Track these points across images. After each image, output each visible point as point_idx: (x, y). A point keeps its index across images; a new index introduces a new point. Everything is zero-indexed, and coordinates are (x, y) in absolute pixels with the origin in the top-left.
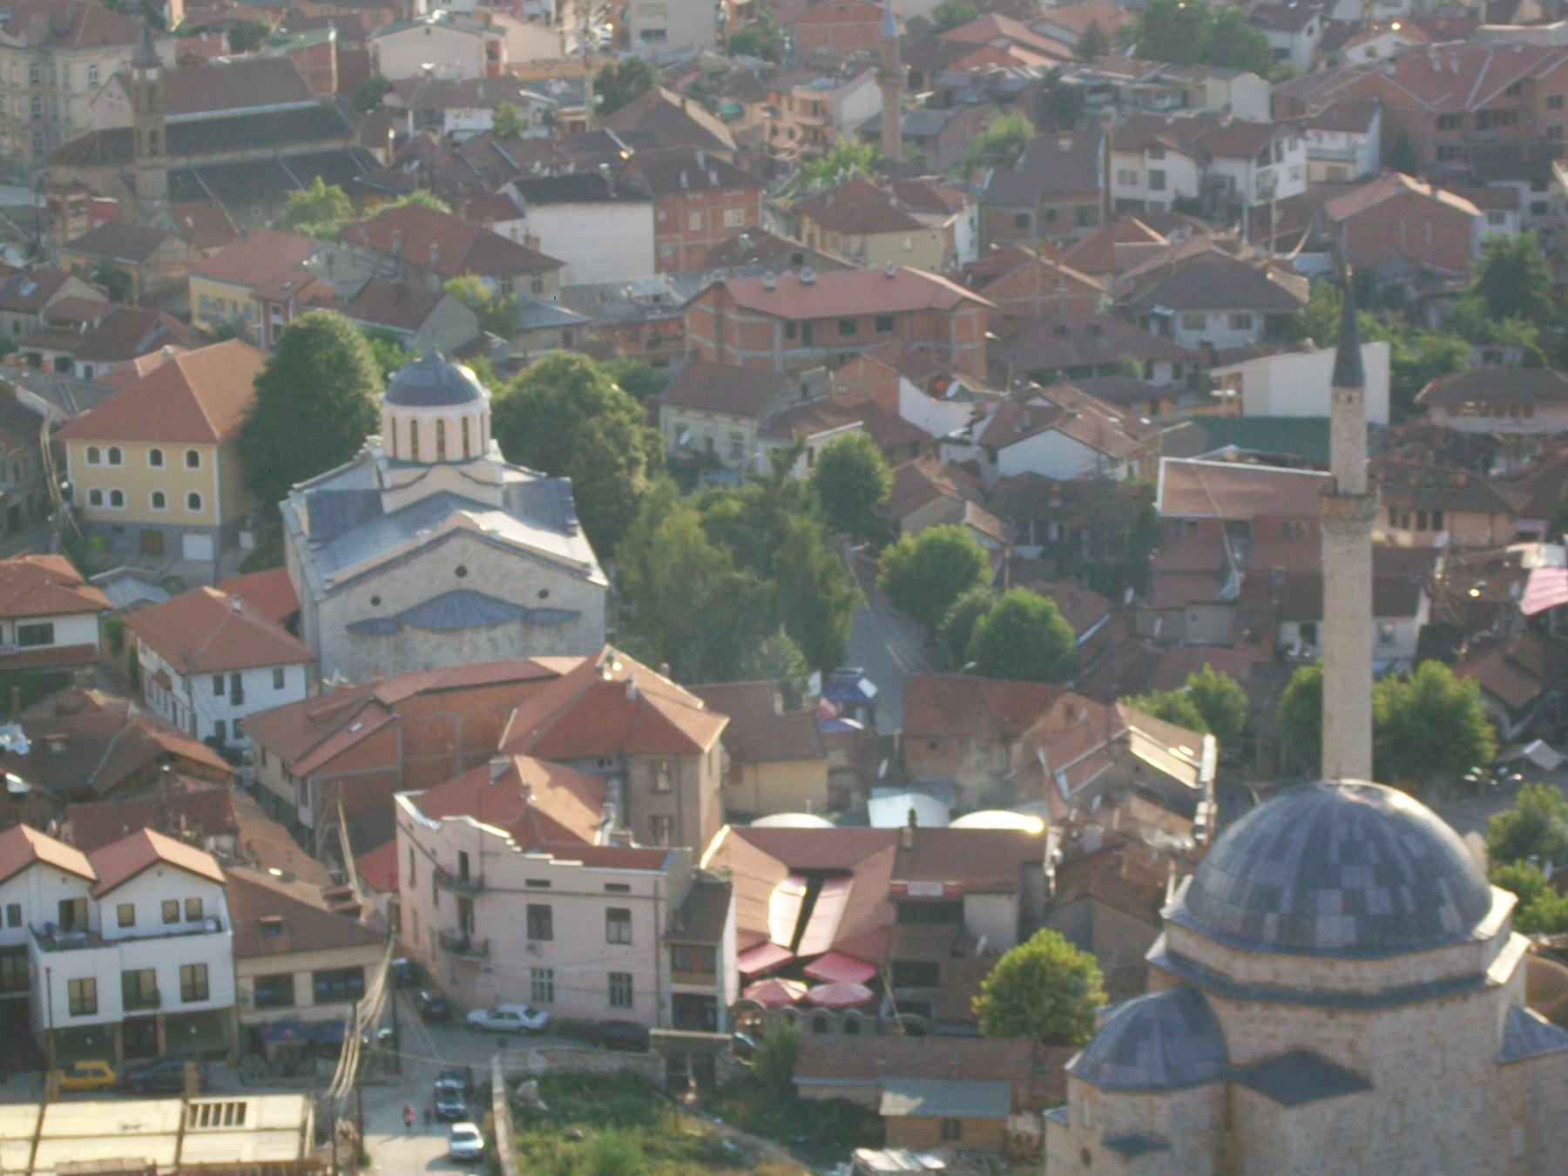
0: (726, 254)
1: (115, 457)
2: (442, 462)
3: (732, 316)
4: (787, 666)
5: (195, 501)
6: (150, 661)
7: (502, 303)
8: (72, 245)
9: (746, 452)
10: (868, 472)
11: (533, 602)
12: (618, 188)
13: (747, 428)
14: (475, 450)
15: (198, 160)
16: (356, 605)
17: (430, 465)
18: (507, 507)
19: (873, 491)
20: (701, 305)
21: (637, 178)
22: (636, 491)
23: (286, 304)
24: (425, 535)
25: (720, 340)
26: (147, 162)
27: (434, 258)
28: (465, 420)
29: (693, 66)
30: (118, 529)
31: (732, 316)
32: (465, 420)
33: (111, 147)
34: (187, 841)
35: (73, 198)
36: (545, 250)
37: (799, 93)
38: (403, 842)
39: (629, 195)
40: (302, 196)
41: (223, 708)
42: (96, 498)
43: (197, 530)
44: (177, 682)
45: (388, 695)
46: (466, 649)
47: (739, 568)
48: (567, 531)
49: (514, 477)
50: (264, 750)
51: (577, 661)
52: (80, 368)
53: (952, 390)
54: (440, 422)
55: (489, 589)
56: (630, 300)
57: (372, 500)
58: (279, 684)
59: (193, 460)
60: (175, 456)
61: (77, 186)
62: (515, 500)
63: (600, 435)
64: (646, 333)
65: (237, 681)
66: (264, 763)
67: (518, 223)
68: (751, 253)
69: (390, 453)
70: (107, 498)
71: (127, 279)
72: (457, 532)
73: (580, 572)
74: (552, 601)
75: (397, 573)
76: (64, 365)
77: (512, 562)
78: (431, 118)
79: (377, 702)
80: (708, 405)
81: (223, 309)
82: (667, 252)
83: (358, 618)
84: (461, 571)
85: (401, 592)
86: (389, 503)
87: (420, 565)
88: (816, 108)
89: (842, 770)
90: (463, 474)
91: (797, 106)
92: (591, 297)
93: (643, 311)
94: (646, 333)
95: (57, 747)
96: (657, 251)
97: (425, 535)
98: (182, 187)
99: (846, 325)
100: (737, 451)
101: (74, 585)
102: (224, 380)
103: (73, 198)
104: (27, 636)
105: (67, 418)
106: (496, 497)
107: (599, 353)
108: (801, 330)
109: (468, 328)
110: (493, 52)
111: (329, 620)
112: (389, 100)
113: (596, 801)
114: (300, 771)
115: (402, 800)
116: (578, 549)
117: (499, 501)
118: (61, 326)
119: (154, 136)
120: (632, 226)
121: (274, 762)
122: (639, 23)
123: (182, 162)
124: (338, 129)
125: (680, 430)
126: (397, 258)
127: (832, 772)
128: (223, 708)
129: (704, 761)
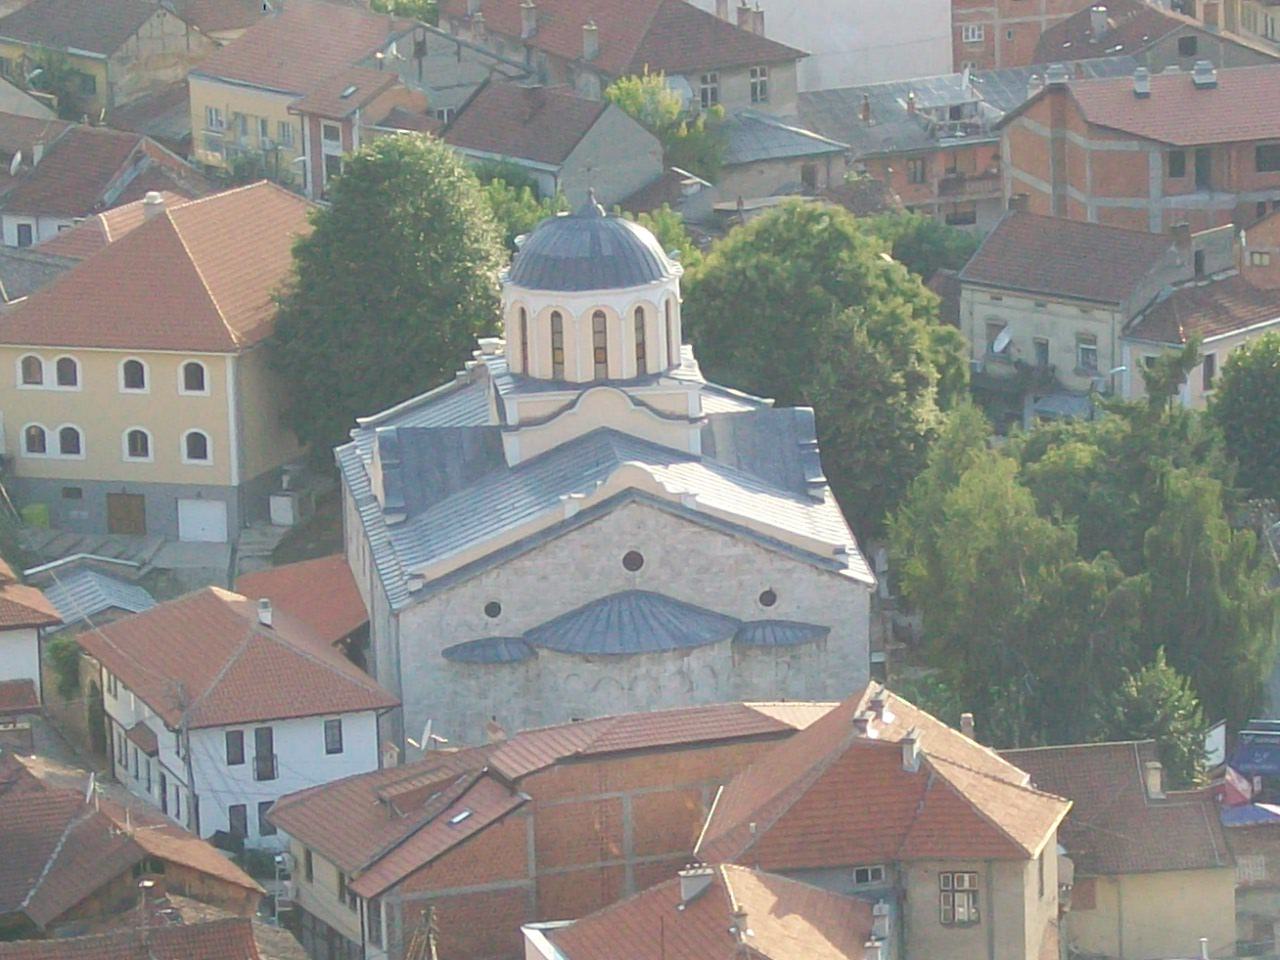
1: (67, 373)
2: (602, 381)
3: (1078, 139)
4: (1167, 718)
5: (197, 446)
6: (122, 707)
9: (1103, 365)
13: (1104, 324)
14: (656, 362)
16: (462, 615)
18: (707, 455)
20: (1027, 122)
23: (348, 121)
24: (573, 502)
25: (1059, 182)
27: (589, 47)
28: (639, 311)
30: (73, 492)
31: (1078, 139)
32: (639, 311)
36: (773, 32)
41: (243, 785)
43: (200, 493)
44: (166, 740)
45: (511, 764)
46: (641, 689)
48: (805, 494)
49: (718, 405)
51: (823, 709)
54: (599, 315)
55: (680, 591)
57: (489, 443)
58: (335, 747)
63: (861, 337)
65: (265, 739)
68: (1111, 37)
69: (518, 369)
70: (53, 440)
71: (88, 82)
72: (628, 495)
73: (828, 562)
75: (527, 563)
77: (718, 546)
79: (493, 774)
80: (1042, 288)
82: (973, 35)
84: (633, 561)
86: (515, 449)
89: (1260, 887)
90: (638, 403)
93: (932, 132)
94: (938, 169)
96: (956, 34)
97: (573, 502)
100: (1087, 363)
102: (246, 248)
107: (860, 201)
108: (1193, 164)
109: (648, 163)
111: (415, 640)
114: (367, 888)
115: (533, 935)
116: (823, 523)
117: (696, 450)
121: (326, 874)
125: (995, 327)
127: (1243, 891)
128: (243, 785)
129: (1032, 868)
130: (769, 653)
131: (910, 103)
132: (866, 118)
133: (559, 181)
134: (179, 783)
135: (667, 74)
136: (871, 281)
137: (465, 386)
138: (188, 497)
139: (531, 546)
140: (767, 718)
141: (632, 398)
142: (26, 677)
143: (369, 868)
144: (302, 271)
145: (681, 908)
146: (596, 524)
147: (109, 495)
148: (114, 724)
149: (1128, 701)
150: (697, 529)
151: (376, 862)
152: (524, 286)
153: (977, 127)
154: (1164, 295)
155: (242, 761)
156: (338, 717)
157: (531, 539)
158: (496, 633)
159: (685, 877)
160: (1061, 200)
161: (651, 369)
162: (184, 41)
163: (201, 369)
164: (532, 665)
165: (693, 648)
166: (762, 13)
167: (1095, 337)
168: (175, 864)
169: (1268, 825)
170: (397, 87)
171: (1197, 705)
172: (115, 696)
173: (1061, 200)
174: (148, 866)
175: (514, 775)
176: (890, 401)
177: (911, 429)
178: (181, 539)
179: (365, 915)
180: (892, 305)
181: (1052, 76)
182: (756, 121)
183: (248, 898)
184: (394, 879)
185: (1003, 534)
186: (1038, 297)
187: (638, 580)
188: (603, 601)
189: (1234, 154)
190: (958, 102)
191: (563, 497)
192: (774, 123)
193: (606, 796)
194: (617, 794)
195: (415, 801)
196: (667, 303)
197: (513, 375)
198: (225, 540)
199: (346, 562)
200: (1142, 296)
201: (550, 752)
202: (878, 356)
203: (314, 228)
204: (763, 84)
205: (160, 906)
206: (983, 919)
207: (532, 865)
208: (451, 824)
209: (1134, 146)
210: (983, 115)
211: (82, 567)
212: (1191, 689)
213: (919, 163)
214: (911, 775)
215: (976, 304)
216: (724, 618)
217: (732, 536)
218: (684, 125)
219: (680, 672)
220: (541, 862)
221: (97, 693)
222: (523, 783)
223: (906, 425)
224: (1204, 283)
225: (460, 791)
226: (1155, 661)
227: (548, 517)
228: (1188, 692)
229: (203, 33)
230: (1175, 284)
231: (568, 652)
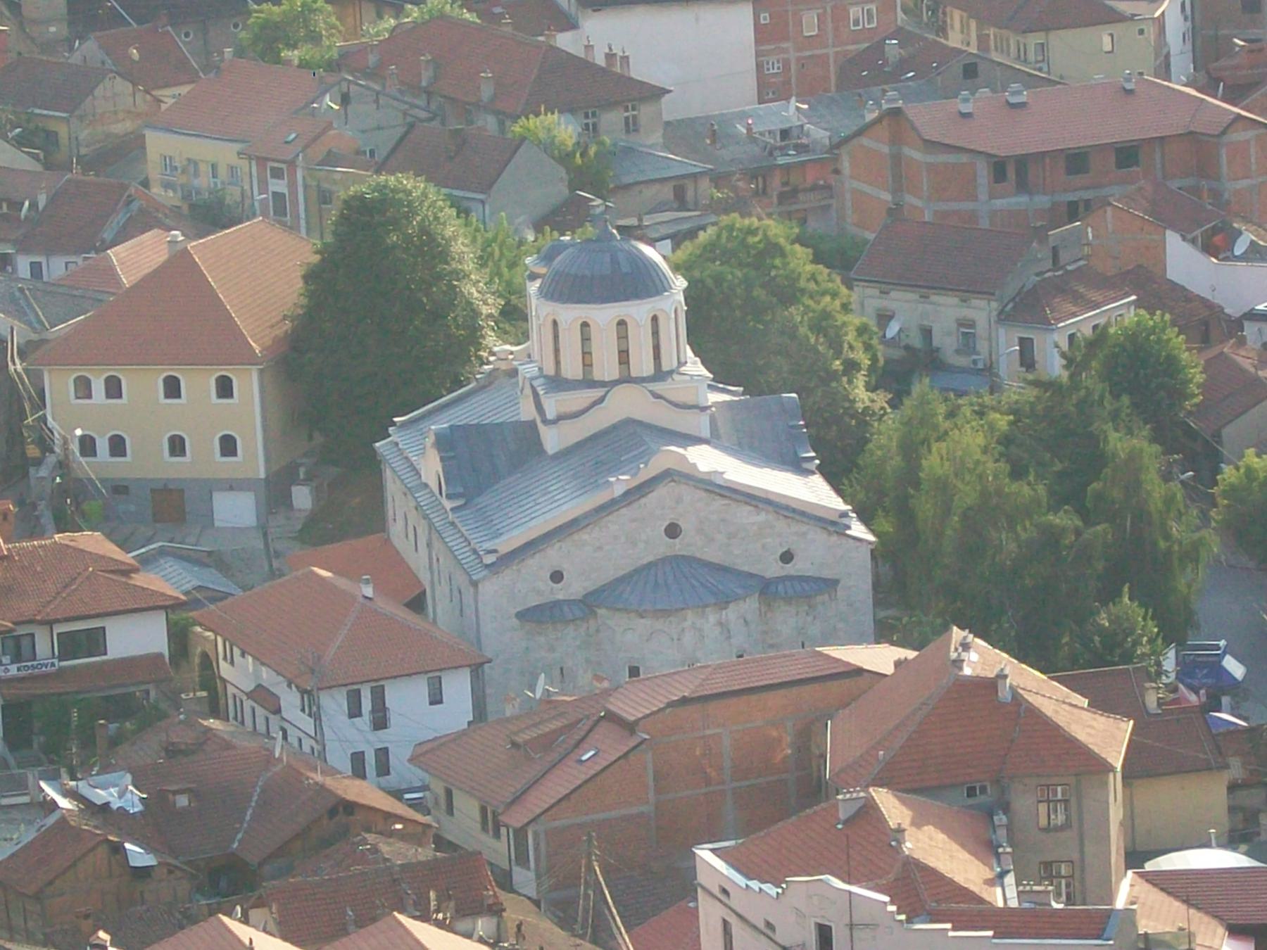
1: (114, 388)
2: (626, 379)
3: (914, 154)
4: (1136, 643)
5: (228, 446)
6: (239, 673)
7: (593, 150)
9: (982, 346)
10: (1171, 366)
11: (774, 569)
13: (982, 311)
16: (529, 585)
17: (615, 383)
18: (713, 439)
19: (1179, 394)
20: (865, 141)
22: (860, 406)
23: (292, 164)
24: (621, 482)
25: (897, 190)
27: (486, 92)
28: (655, 319)
30: (120, 489)
31: (914, 154)
32: (655, 319)
34: (440, 925)
36: (640, 71)
38: (709, 915)
42: (88, 446)
43: (232, 486)
46: (689, 639)
47: (1054, 508)
48: (798, 466)
49: (714, 398)
50: (449, 793)
52: (23, 265)
53: (1240, 248)
54: (622, 323)
55: (712, 554)
57: (527, 436)
58: (436, 699)
59: (225, 388)
60: (199, 384)
63: (803, 330)
64: (776, 182)
65: (379, 697)
66: (450, 810)
68: (903, 65)
69: (550, 370)
70: (103, 446)
72: (666, 475)
74: (799, 567)
75: (584, 536)
77: (745, 516)
79: (612, 717)
80: (925, 283)
81: (196, 174)
83: (533, 601)
84: (673, 531)
85: (590, 562)
86: (552, 440)
90: (657, 396)
92: (698, 134)
94: (776, 182)
95: (183, 801)
96: (759, 66)
97: (621, 482)
99: (1076, 161)
100: (968, 341)
101: (127, 572)
102: (262, 274)
104: (71, 645)
105: (34, 337)
106: (701, 424)
109: (555, 189)
113: (987, 849)
114: (516, 818)
115: (704, 854)
116: (815, 491)
117: (706, 433)
121: (467, 808)
125: (884, 318)
127: (1232, 788)
130: (790, 604)
131: (749, 129)
132: (713, 142)
133: (487, 207)
134: (302, 735)
135: (560, 112)
136: (802, 283)
137: (484, 387)
138: (221, 490)
139: (586, 522)
140: (838, 660)
141: (650, 391)
142: (156, 651)
143: (513, 802)
144: (311, 295)
145: (840, 826)
146: (643, 500)
147: (152, 490)
148: (230, 688)
149: (1101, 630)
150: (727, 502)
151: (518, 798)
152: (556, 301)
153: (807, 146)
154: (1029, 286)
155: (360, 714)
156: (437, 674)
157: (586, 515)
158: (560, 597)
159: (843, 800)
161: (665, 368)
162: (131, 99)
163: (119, 381)
164: (592, 622)
165: (728, 603)
166: (627, 57)
167: (974, 322)
168: (363, 806)
169: (1232, 732)
170: (332, 132)
171: (1158, 633)
172: (232, 663)
174: (341, 809)
175: (632, 718)
176: (834, 384)
177: (852, 407)
178: (217, 524)
179: (512, 843)
180: (822, 304)
181: (888, 101)
182: (631, 148)
183: (424, 833)
184: (538, 811)
185: (984, 495)
186: (883, 286)
187: (677, 547)
188: (650, 565)
189: (1047, 160)
190: (786, 126)
191: (612, 479)
192: (644, 150)
193: (708, 732)
194: (719, 730)
195: (547, 743)
196: (676, 311)
197: (546, 377)
198: (254, 524)
199: (388, 541)
200: (1011, 289)
201: (661, 698)
202: (820, 348)
203: (318, 257)
204: (634, 117)
205: (359, 844)
206: (1075, 824)
207: (651, 794)
208: (581, 762)
209: (964, 158)
210: (808, 135)
211: (162, 552)
212: (1152, 619)
213: (760, 179)
214: (1004, 705)
216: (752, 575)
217: (756, 507)
218: (578, 155)
219: (720, 624)
220: (658, 791)
221: (207, 663)
222: (641, 723)
223: (847, 405)
224: (1060, 273)
225: (583, 733)
226: (1120, 595)
227: (600, 497)
228: (1150, 623)
229: (147, 92)
230: (1037, 275)
231: (626, 610)
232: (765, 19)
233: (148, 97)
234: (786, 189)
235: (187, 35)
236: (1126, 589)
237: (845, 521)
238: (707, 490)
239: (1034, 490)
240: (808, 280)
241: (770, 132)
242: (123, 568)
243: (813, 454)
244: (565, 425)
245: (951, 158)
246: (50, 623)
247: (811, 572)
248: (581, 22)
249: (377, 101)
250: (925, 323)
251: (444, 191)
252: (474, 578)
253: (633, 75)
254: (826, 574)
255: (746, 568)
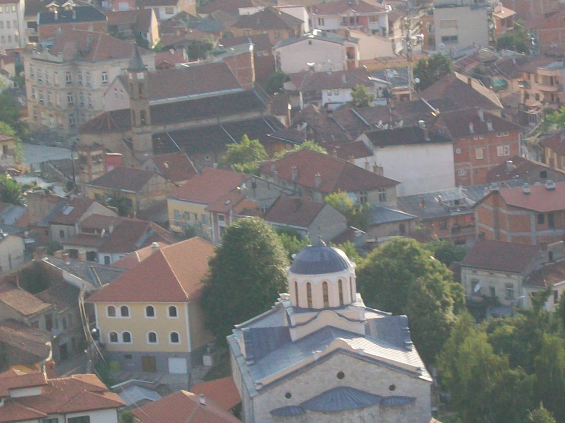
0: (500, 173)
1: (125, 312)
2: (327, 308)
3: (503, 211)
5: (175, 337)
8: (95, 183)
9: (516, 295)
11: (386, 393)
12: (430, 135)
13: (516, 280)
14: (347, 300)
15: (171, 127)
16: (276, 398)
18: (367, 335)
21: (442, 128)
22: (448, 322)
23: (228, 214)
24: (317, 354)
26: (139, 130)
27: (318, 182)
28: (340, 281)
29: (475, 57)
30: (128, 356)
31: (503, 211)
32: (340, 281)
33: (117, 121)
35: (94, 153)
36: (387, 174)
37: (542, 72)
39: (437, 139)
40: (236, 147)
42: (114, 338)
43: (177, 355)
49: (371, 316)
52: (101, 258)
54: (325, 283)
55: (358, 386)
56: (441, 204)
57: (285, 332)
59: (173, 312)
61: (96, 146)
62: (372, 330)
63: (424, 288)
67: (369, 159)
68: (514, 172)
69: (294, 304)
70: (120, 337)
71: (129, 202)
72: (338, 351)
73: (414, 373)
74: (398, 392)
75: (300, 377)
76: (91, 256)
77: (373, 369)
78: (314, 96)
81: (189, 219)
82: (463, 173)
83: (278, 406)
84: (341, 375)
85: (304, 389)
86: (295, 335)
87: (315, 372)
88: (552, 81)
90: (340, 315)
91: (540, 80)
93: (448, 210)
96: (456, 173)
97: (317, 354)
98: (162, 145)
100: (510, 294)
101: (102, 392)
102: (190, 262)
103: (94, 153)
105: (94, 289)
106: (361, 329)
107: (421, 237)
109: (341, 226)
110: (351, 54)
112: (287, 86)
116: (412, 359)
117: (363, 332)
118: (89, 233)
119: (143, 114)
120: (442, 156)
122: (440, 33)
123: (160, 129)
124: (257, 105)
125: (474, 283)
126: (295, 183)
131: (439, 199)
136: (427, 267)
144: (212, 270)
157: (302, 368)
160: (498, 234)
173: (498, 234)
176: (436, 312)
192: (387, 208)
196: (350, 278)
204: (384, 194)
209: (524, 213)
211: (132, 384)
215: (467, 274)
216: (376, 396)
217: (378, 365)
219: (360, 417)
227: (307, 360)
232: (458, 151)
233: (173, 185)
234: (456, 226)
235: (207, 158)
236: (541, 404)
237: (419, 372)
238: (355, 358)
239: (503, 359)
240: (429, 265)
241: (450, 201)
242: (100, 390)
243: (411, 342)
244: (300, 329)
245: (519, 213)
246: (64, 414)
247: (404, 394)
248: (374, 152)
249: (268, 187)
250: (492, 285)
251: (272, 223)
252: (252, 395)
253: (385, 176)
254: (410, 395)
255: (373, 393)
